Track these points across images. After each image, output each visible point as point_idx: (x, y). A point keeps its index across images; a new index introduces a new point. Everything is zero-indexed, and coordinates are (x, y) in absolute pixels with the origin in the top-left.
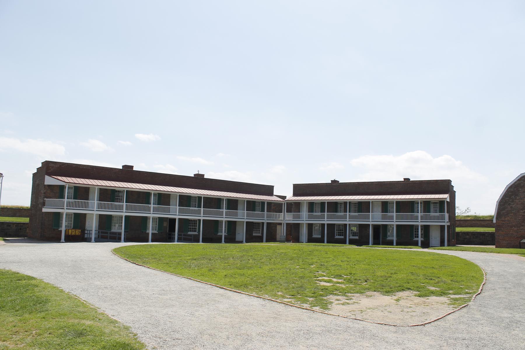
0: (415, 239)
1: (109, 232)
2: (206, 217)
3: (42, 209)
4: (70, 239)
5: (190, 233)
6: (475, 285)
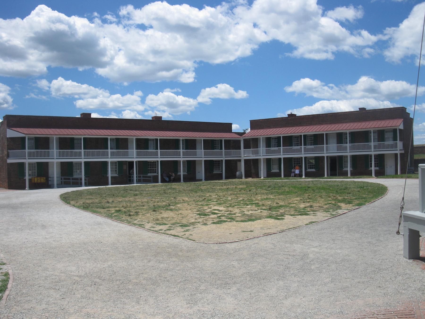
0: (377, 168)
1: (71, 178)
2: (361, 152)
3: (6, 161)
4: (34, 186)
5: (149, 175)
6: (210, 214)
